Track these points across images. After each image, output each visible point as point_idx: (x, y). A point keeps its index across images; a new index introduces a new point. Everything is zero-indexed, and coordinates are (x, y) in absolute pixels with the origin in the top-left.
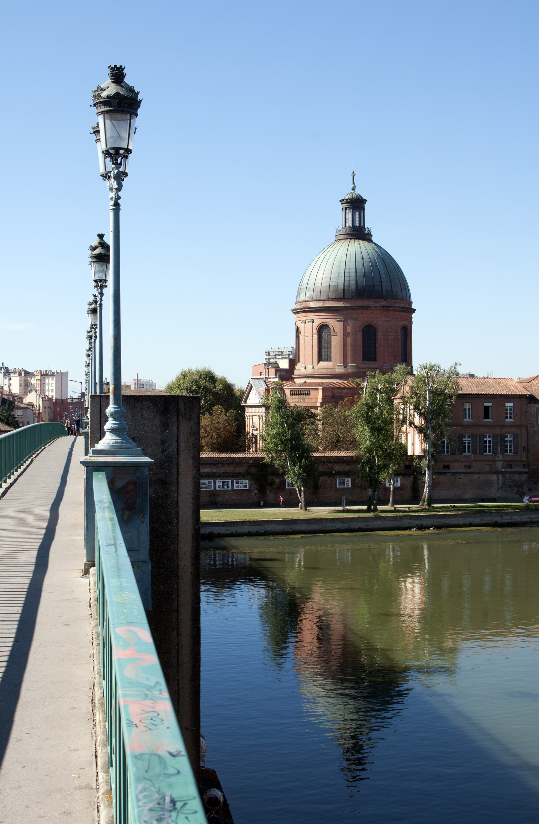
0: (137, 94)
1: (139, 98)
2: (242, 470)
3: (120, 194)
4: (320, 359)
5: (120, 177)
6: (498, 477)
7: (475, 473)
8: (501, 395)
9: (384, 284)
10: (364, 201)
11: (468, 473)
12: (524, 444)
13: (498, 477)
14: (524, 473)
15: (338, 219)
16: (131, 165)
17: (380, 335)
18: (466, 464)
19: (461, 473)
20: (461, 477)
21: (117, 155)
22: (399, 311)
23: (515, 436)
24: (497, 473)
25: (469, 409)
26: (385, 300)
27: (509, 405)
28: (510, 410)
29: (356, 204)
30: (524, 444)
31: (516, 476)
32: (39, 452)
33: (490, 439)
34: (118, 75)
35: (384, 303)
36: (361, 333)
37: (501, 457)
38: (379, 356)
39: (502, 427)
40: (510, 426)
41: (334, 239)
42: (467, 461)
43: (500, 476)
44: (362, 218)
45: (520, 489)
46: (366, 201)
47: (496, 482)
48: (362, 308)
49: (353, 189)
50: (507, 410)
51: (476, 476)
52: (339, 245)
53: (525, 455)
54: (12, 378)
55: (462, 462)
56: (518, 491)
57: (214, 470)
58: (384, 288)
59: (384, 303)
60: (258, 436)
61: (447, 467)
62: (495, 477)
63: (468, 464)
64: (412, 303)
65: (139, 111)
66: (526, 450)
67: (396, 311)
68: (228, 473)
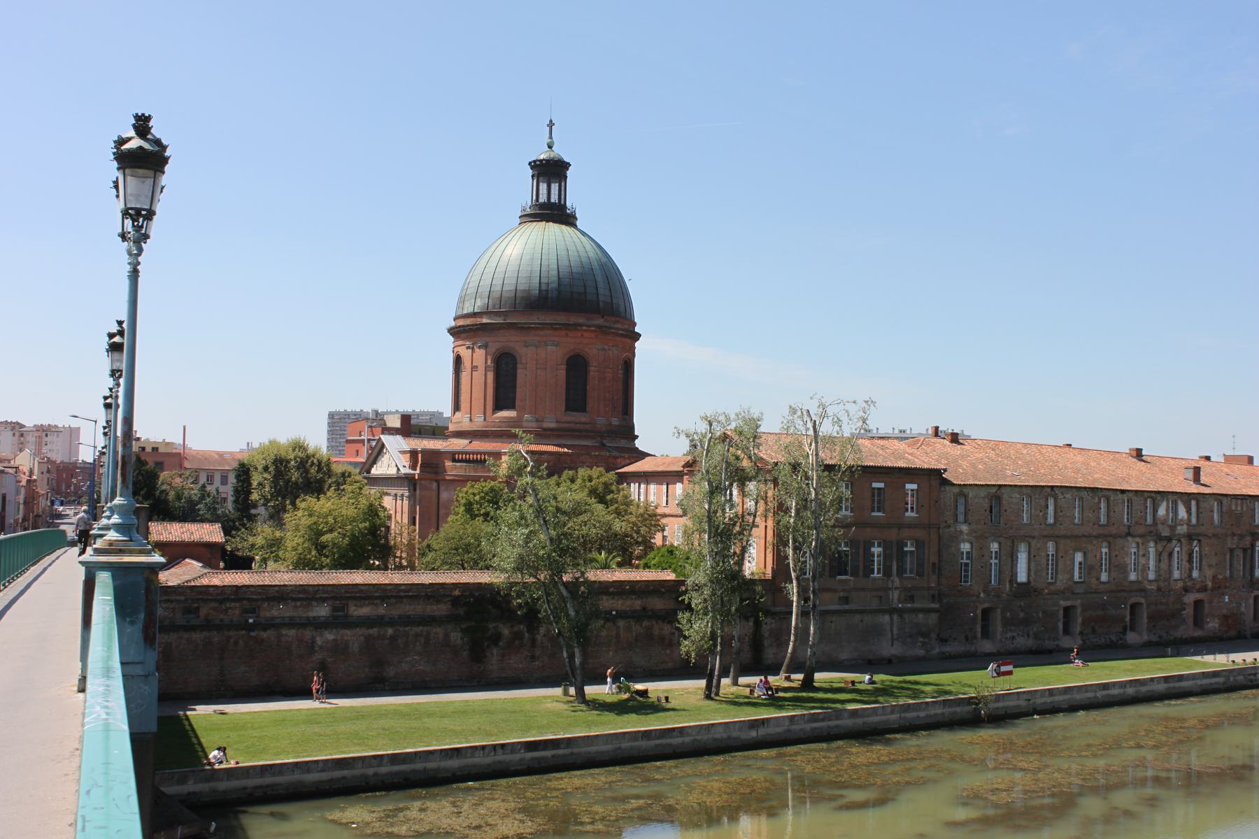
0: (164, 148)
1: (167, 154)
2: (442, 609)
3: (140, 259)
4: (498, 407)
5: (141, 238)
6: (892, 619)
7: (856, 612)
8: (900, 469)
9: (601, 291)
10: (566, 166)
11: (846, 612)
12: (934, 559)
13: (892, 619)
15: (523, 190)
16: (156, 228)
17: (593, 372)
18: (842, 594)
20: (834, 619)
21: (139, 219)
22: (622, 335)
23: (919, 544)
24: (892, 611)
27: (910, 486)
29: (551, 171)
30: (934, 559)
31: (921, 616)
33: (880, 549)
34: (142, 125)
35: (600, 321)
36: (564, 367)
37: (897, 582)
38: (591, 404)
39: (900, 526)
40: (913, 525)
41: (518, 221)
42: (843, 590)
43: (895, 617)
44: (562, 192)
46: (332, 416)
47: (888, 628)
48: (567, 326)
49: (550, 147)
51: (858, 617)
52: (529, 231)
53: (934, 577)
55: (835, 591)
56: (924, 644)
57: (382, 610)
58: (601, 298)
59: (600, 321)
60: (979, 635)
62: (886, 618)
65: (167, 168)
66: (937, 568)
67: (617, 334)
68: (409, 617)
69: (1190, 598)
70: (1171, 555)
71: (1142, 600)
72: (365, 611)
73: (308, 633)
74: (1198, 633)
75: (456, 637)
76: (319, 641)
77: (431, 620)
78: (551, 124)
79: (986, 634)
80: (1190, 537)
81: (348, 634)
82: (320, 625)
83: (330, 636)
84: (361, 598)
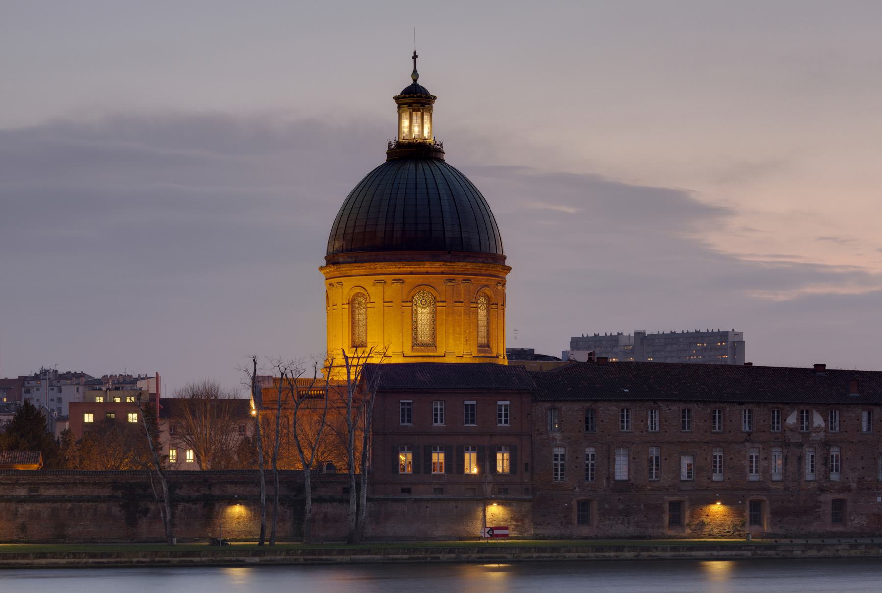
2: (106, 492)
7: (449, 500)
14: (525, 500)
18: (436, 486)
19: (428, 500)
25: (441, 410)
26: (450, 253)
28: (506, 410)
32: (339, 558)
45: (520, 524)
46: (742, 333)
50: (500, 410)
54: (63, 388)
57: (63, 492)
58: (448, 234)
61: (409, 491)
63: (440, 486)
64: (505, 258)
69: (827, 498)
70: (800, 459)
71: (765, 498)
72: (51, 492)
73: (13, 506)
74: (839, 528)
75: (116, 510)
76: (20, 510)
77: (98, 499)
78: (415, 57)
79: (584, 519)
80: (827, 444)
81: (40, 506)
82: (21, 501)
83: (28, 507)
84: (48, 484)
